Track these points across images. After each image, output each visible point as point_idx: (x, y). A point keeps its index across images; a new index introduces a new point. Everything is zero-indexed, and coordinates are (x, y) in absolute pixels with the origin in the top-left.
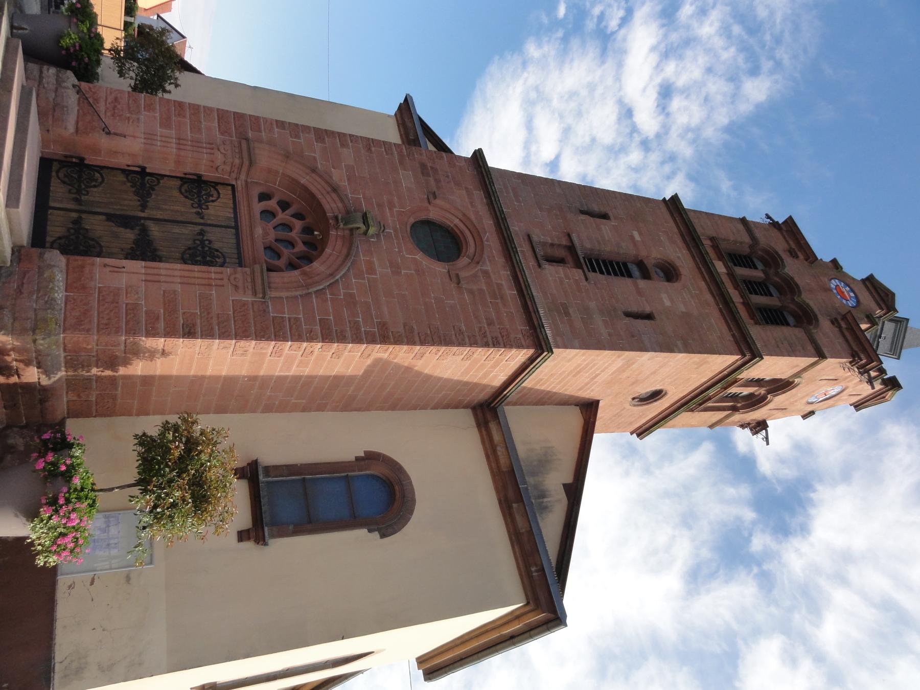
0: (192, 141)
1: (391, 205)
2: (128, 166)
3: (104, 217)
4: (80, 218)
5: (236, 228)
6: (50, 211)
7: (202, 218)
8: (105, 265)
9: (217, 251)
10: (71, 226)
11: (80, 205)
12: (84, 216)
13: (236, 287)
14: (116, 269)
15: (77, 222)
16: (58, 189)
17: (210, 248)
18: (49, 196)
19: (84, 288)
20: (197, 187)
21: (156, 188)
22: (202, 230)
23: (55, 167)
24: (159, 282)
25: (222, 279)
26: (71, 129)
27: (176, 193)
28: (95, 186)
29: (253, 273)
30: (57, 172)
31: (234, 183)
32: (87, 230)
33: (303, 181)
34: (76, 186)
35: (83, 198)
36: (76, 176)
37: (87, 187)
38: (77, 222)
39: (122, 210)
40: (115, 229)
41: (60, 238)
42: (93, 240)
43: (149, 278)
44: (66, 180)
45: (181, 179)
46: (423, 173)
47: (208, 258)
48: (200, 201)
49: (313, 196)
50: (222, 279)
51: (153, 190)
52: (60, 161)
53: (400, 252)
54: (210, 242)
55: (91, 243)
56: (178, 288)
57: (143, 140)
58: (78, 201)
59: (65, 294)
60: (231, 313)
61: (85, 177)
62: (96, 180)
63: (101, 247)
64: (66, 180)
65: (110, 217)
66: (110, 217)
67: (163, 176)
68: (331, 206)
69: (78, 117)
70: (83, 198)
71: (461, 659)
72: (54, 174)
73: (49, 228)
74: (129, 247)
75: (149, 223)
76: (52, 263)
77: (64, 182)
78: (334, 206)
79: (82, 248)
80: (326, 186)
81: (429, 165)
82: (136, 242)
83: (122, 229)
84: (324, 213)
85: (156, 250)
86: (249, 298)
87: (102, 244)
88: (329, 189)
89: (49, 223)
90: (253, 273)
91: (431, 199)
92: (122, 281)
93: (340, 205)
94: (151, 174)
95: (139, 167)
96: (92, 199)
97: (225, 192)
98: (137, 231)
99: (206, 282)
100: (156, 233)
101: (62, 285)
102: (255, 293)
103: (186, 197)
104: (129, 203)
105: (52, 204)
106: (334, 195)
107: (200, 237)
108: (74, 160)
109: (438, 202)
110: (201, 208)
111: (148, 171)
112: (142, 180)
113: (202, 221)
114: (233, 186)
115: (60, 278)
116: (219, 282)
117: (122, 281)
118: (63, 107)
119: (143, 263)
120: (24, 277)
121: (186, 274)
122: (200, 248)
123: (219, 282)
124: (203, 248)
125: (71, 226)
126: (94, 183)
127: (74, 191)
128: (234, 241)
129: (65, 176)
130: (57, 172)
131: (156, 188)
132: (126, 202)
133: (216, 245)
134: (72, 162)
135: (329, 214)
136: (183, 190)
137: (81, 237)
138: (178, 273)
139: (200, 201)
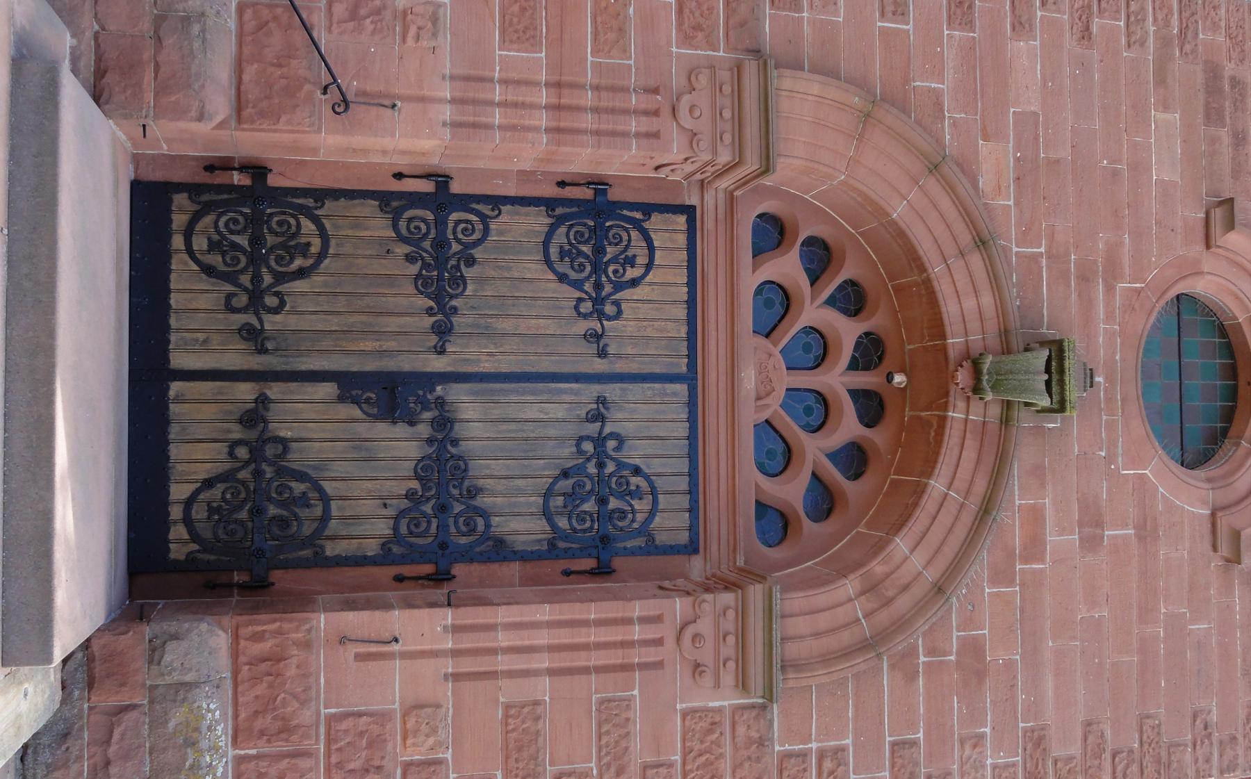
0: (597, 88)
1: (1113, 272)
2: (399, 176)
3: (328, 389)
4: (263, 400)
5: (690, 378)
6: (175, 387)
7: (602, 354)
8: (343, 640)
9: (637, 471)
10: (237, 433)
11: (262, 350)
12: (275, 390)
13: (697, 668)
14: (374, 648)
15: (254, 417)
16: (193, 296)
17: (620, 465)
18: (167, 328)
19: (286, 729)
20: (595, 225)
21: (477, 253)
22: (601, 400)
23: (181, 210)
24: (493, 675)
25: (659, 642)
26: (220, 105)
27: (533, 268)
28: (302, 273)
29: (742, 613)
30: (188, 234)
31: (694, 200)
32: (284, 442)
33: (899, 211)
34: (245, 279)
35: (271, 322)
36: (243, 241)
37: (280, 278)
38: (254, 417)
39: (382, 353)
40: (365, 429)
41: (208, 483)
42: (301, 476)
43: (468, 665)
44: (216, 260)
45: (550, 204)
46: (1207, 116)
47: (613, 503)
48: (598, 286)
49: (915, 261)
50: (659, 642)
51: (471, 262)
52: (193, 190)
53: (1110, 459)
54: (620, 440)
55: (299, 487)
56: (543, 688)
57: (447, 113)
58: (254, 337)
59: (231, 753)
60: (677, 758)
61: (270, 240)
62: (304, 249)
63: (325, 499)
64: (216, 260)
65: (350, 385)
66: (350, 385)
67: (497, 201)
68: (966, 312)
69: (240, 44)
70: (271, 322)
71: (732, 304)
72: (178, 241)
73: (175, 451)
74: (401, 488)
75: (456, 393)
76: (189, 678)
77: (208, 270)
78: (969, 304)
79: (273, 511)
80: (960, 228)
81: (1229, 69)
82: (423, 471)
83: (382, 429)
84: (938, 328)
85: (474, 492)
86: (725, 700)
87: (328, 487)
88: (966, 238)
89: (174, 431)
90: (742, 613)
91: (1217, 228)
92: (392, 687)
93: (987, 300)
94: (465, 202)
95: (427, 176)
96: (293, 322)
97: (668, 234)
98: (424, 430)
99: (615, 657)
100: (476, 430)
101: (222, 734)
102: (743, 684)
103: (562, 278)
104: (398, 335)
105: (179, 360)
106: (976, 261)
107: (593, 429)
108: (237, 178)
109: (1235, 239)
110: (601, 315)
111: (456, 188)
112: (437, 220)
113: (600, 366)
114: (689, 211)
115: (214, 712)
116: (651, 655)
117: (392, 687)
118: (186, 20)
119: (448, 616)
120: (107, 742)
121: (564, 636)
122: (592, 469)
123: (651, 655)
124: (601, 465)
125: (237, 433)
126: (298, 263)
127: (243, 300)
128: (682, 430)
129: (213, 246)
130: (188, 234)
131: (477, 253)
132: (393, 323)
133: (635, 454)
134: (231, 188)
135: (955, 342)
136: (554, 251)
137: (269, 472)
138: (543, 638)
139: (598, 286)
